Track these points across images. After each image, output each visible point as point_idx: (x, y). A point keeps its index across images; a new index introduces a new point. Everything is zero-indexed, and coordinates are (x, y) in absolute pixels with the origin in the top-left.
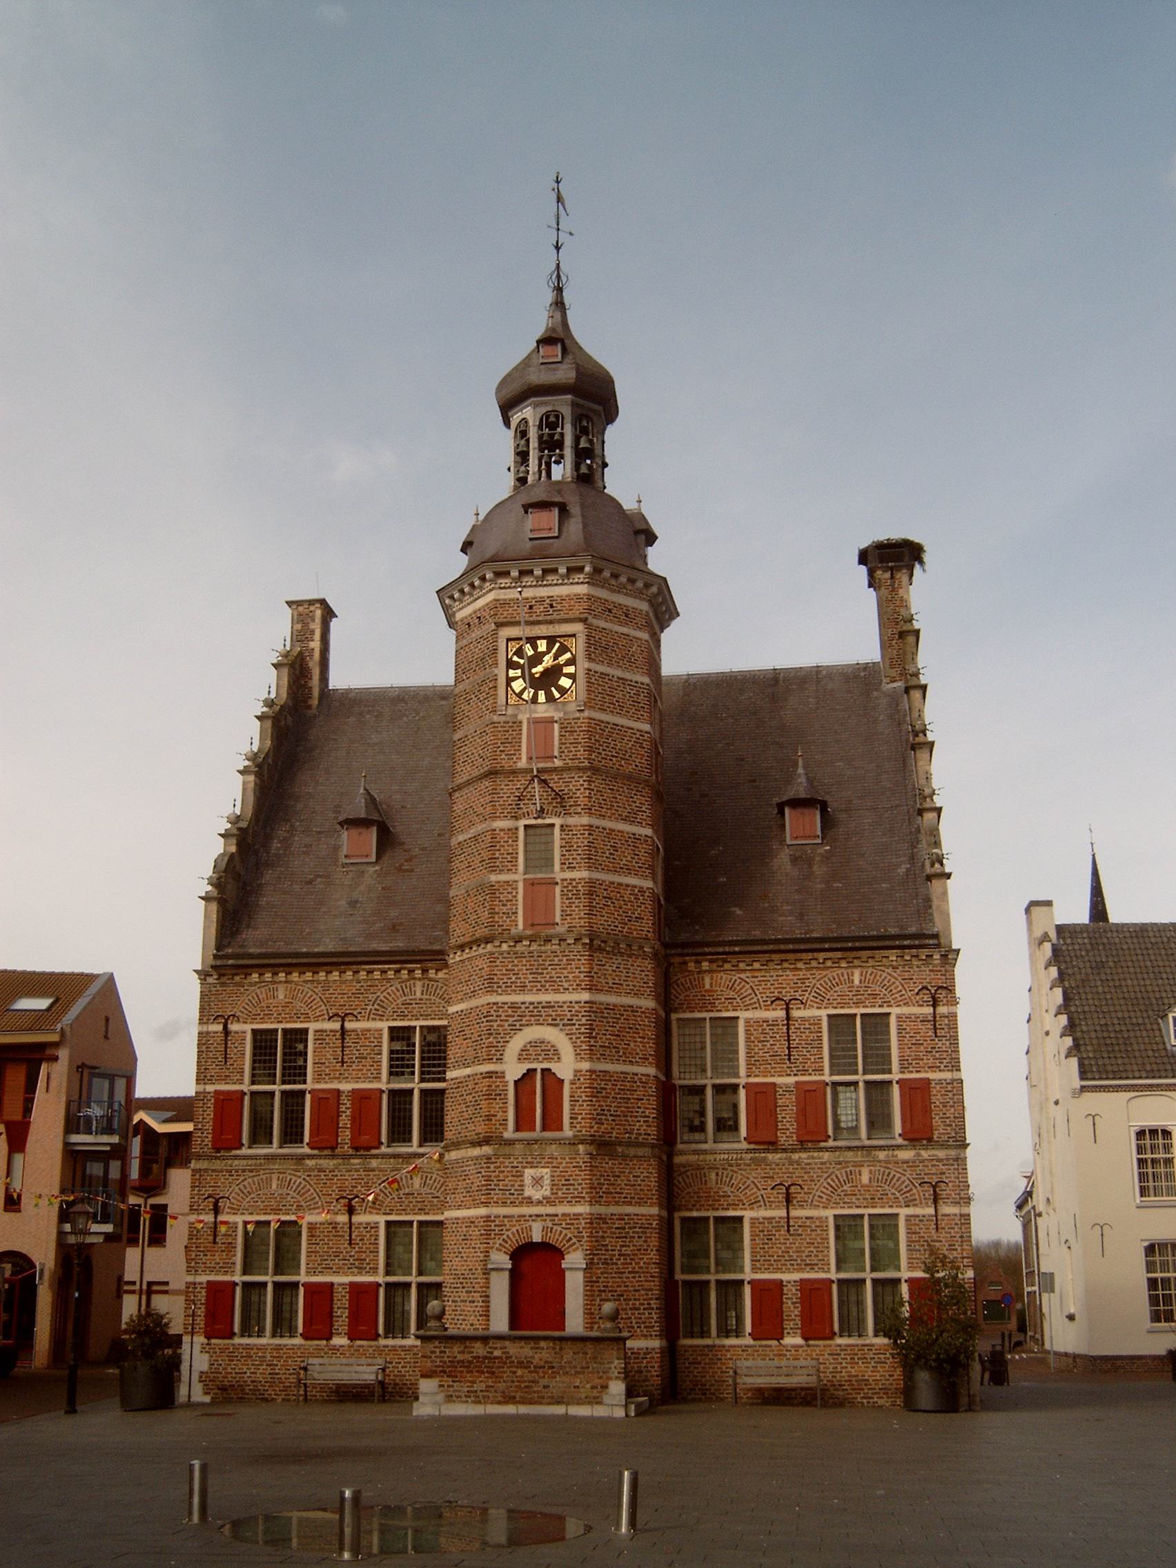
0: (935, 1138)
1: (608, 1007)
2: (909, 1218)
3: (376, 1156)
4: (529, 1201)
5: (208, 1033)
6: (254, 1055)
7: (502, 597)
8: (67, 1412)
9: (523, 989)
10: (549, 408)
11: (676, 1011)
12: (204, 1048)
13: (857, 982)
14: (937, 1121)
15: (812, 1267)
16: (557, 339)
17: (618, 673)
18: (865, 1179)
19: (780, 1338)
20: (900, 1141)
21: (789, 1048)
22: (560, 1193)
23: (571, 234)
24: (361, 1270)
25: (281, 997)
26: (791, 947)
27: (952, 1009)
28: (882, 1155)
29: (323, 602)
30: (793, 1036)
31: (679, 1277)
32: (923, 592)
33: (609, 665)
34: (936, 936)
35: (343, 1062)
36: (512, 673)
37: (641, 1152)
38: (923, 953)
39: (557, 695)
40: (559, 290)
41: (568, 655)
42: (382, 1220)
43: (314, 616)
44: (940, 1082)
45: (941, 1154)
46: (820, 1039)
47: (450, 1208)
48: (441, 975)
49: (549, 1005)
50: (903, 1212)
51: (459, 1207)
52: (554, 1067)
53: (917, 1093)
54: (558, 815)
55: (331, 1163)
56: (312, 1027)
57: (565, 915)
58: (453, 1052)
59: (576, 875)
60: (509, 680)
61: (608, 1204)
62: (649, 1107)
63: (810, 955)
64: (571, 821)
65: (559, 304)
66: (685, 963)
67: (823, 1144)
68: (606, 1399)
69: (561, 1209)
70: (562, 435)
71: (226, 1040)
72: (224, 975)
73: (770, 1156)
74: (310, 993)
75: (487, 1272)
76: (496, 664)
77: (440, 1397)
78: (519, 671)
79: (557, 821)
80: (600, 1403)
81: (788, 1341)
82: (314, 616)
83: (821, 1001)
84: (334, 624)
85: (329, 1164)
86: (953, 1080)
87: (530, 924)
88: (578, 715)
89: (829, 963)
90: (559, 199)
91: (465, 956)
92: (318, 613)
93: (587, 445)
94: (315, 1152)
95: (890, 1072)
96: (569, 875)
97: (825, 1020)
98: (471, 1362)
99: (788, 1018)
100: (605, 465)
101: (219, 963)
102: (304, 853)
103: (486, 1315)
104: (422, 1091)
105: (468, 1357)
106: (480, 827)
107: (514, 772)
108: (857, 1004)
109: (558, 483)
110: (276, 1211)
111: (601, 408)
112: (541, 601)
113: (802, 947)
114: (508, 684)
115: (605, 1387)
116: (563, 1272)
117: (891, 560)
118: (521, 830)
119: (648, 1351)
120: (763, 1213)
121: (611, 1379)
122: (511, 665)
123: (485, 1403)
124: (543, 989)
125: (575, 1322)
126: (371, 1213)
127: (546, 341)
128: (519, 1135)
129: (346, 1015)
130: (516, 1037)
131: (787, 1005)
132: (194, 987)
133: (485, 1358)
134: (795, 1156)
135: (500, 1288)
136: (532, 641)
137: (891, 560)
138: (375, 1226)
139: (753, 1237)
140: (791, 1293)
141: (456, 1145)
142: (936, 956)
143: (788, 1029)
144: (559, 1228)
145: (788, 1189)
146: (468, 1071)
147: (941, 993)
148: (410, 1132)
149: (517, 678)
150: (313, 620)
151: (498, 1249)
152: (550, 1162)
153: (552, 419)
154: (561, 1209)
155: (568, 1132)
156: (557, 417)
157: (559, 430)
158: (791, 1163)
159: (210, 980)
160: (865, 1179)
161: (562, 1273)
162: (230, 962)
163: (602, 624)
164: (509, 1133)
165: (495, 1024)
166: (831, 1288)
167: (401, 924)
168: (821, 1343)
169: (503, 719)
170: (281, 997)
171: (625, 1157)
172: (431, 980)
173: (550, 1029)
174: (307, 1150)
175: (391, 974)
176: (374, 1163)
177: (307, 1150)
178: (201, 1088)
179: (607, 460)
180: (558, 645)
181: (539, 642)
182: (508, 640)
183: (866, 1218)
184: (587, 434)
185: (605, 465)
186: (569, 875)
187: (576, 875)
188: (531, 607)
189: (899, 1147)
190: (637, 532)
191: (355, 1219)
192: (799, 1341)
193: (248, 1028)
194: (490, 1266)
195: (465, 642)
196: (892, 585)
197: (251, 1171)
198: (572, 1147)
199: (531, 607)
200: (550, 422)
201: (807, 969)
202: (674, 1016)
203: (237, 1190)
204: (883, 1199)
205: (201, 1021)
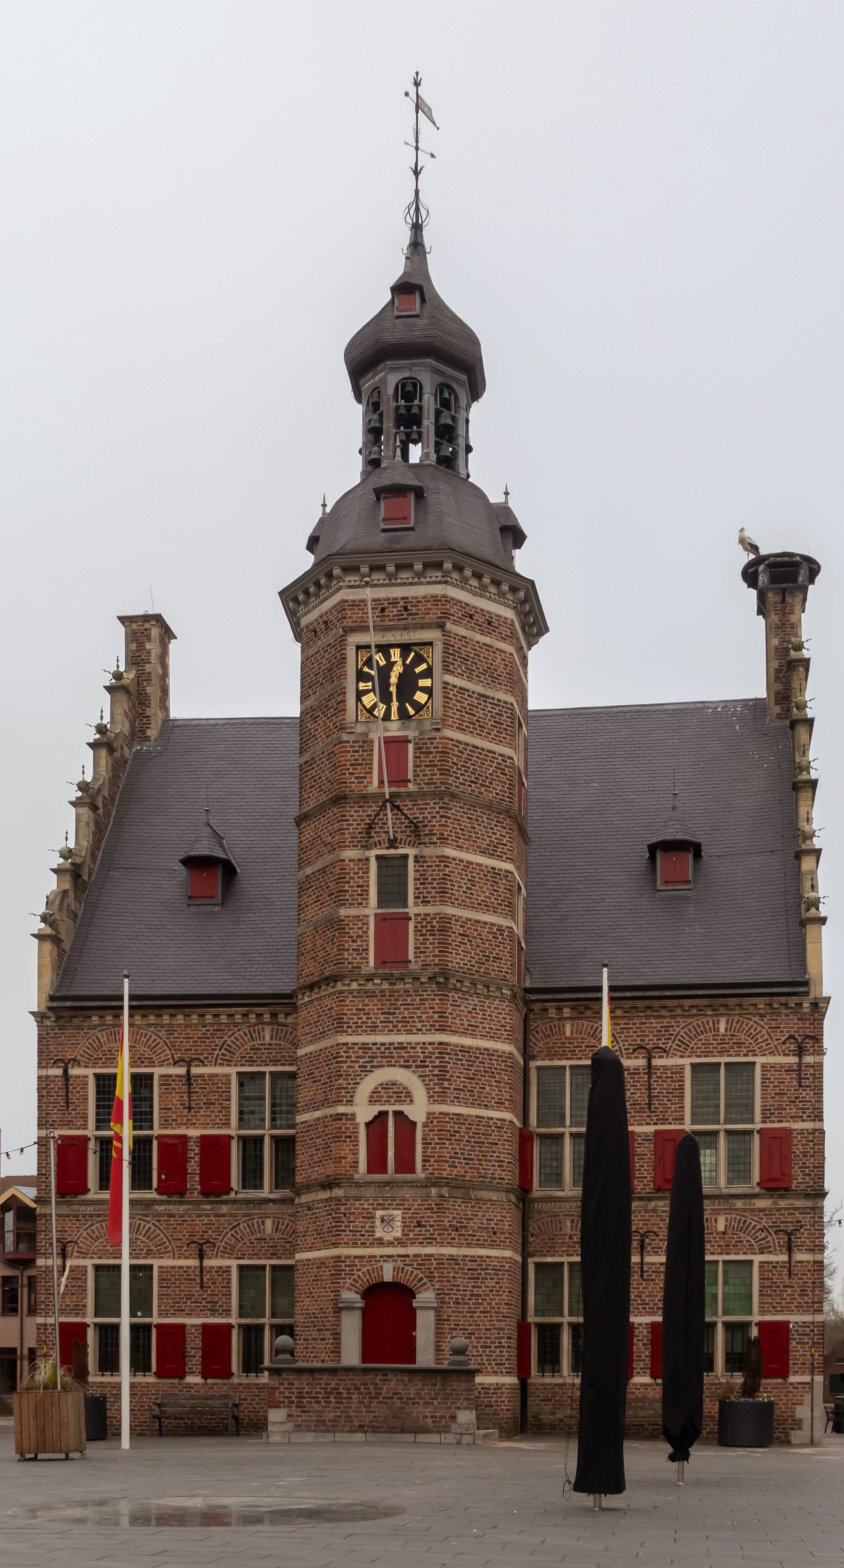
0: (794, 1187)
2: (762, 1264)
4: (380, 1242)
5: (48, 1077)
6: (98, 1100)
7: (351, 597)
9: (374, 1029)
10: (407, 374)
11: (533, 1058)
12: (44, 1093)
13: (722, 1030)
14: (796, 1170)
16: (412, 288)
17: (480, 689)
20: (757, 1190)
21: (649, 1097)
22: (411, 1234)
23: (433, 156)
24: (213, 1312)
27: (817, 1059)
28: (739, 1204)
29: (158, 619)
30: (655, 1085)
31: (532, 1318)
32: (818, 619)
33: (470, 679)
35: (190, 1108)
36: (362, 686)
37: (494, 1196)
38: (793, 1001)
39: (412, 711)
40: (417, 228)
41: (424, 666)
42: (234, 1264)
43: (147, 636)
45: (798, 1204)
46: (681, 1087)
47: (302, 1250)
48: (290, 1020)
49: (401, 1047)
50: (757, 1259)
51: (310, 1249)
53: (777, 1145)
54: (412, 844)
55: (182, 1208)
56: (157, 1071)
58: (304, 1095)
59: (430, 909)
60: (360, 694)
61: (460, 1246)
62: (506, 1151)
63: (675, 1002)
65: (417, 247)
66: (545, 1010)
69: (412, 1250)
71: (67, 1085)
72: (62, 1017)
74: (154, 1037)
75: (338, 1310)
76: (344, 675)
77: (289, 1426)
78: (370, 684)
79: (411, 852)
81: (191, 1379)
82: (147, 636)
83: (684, 1049)
84: (173, 645)
86: (815, 1130)
87: (381, 962)
89: (694, 1011)
90: (419, 106)
91: (314, 996)
92: (155, 632)
93: (449, 422)
94: (164, 1197)
95: (752, 1121)
96: (423, 910)
100: (469, 449)
101: (55, 1004)
103: (337, 1351)
104: (272, 1137)
106: (327, 859)
107: (365, 798)
108: (721, 1053)
109: (415, 466)
111: (464, 377)
112: (394, 602)
113: (668, 993)
114: (359, 699)
115: (453, 1418)
116: (413, 1311)
118: (373, 865)
119: (498, 1387)
122: (361, 676)
123: (334, 1432)
125: (425, 1357)
126: (223, 1257)
127: (402, 289)
129: (193, 1060)
130: (368, 1078)
131: (649, 1052)
132: (32, 1029)
134: (652, 1205)
135: (351, 1330)
136: (384, 649)
138: (228, 1270)
141: (308, 1187)
143: (649, 1078)
144: (410, 1268)
146: (318, 1114)
147: (809, 1042)
148: (261, 1178)
149: (366, 692)
150: (149, 639)
151: (348, 1289)
153: (409, 388)
154: (412, 1250)
156: (414, 385)
157: (416, 402)
159: (48, 1023)
161: (412, 1314)
162: (68, 1004)
163: (462, 631)
165: (345, 1065)
169: (352, 738)
171: (478, 1200)
173: (402, 1071)
175: (238, 1018)
176: (225, 1209)
178: (43, 1133)
179: (472, 443)
180: (413, 654)
181: (392, 651)
182: (359, 648)
183: (721, 1264)
184: (449, 408)
185: (469, 449)
186: (423, 910)
187: (430, 909)
188: (383, 610)
190: (504, 530)
191: (207, 1263)
193: (90, 1072)
194: (341, 1305)
195: (311, 652)
197: (99, 1216)
198: (425, 1190)
199: (383, 610)
200: (409, 391)
201: (672, 1017)
202: (533, 1064)
203: (85, 1234)
204: (737, 1247)
205: (40, 1066)
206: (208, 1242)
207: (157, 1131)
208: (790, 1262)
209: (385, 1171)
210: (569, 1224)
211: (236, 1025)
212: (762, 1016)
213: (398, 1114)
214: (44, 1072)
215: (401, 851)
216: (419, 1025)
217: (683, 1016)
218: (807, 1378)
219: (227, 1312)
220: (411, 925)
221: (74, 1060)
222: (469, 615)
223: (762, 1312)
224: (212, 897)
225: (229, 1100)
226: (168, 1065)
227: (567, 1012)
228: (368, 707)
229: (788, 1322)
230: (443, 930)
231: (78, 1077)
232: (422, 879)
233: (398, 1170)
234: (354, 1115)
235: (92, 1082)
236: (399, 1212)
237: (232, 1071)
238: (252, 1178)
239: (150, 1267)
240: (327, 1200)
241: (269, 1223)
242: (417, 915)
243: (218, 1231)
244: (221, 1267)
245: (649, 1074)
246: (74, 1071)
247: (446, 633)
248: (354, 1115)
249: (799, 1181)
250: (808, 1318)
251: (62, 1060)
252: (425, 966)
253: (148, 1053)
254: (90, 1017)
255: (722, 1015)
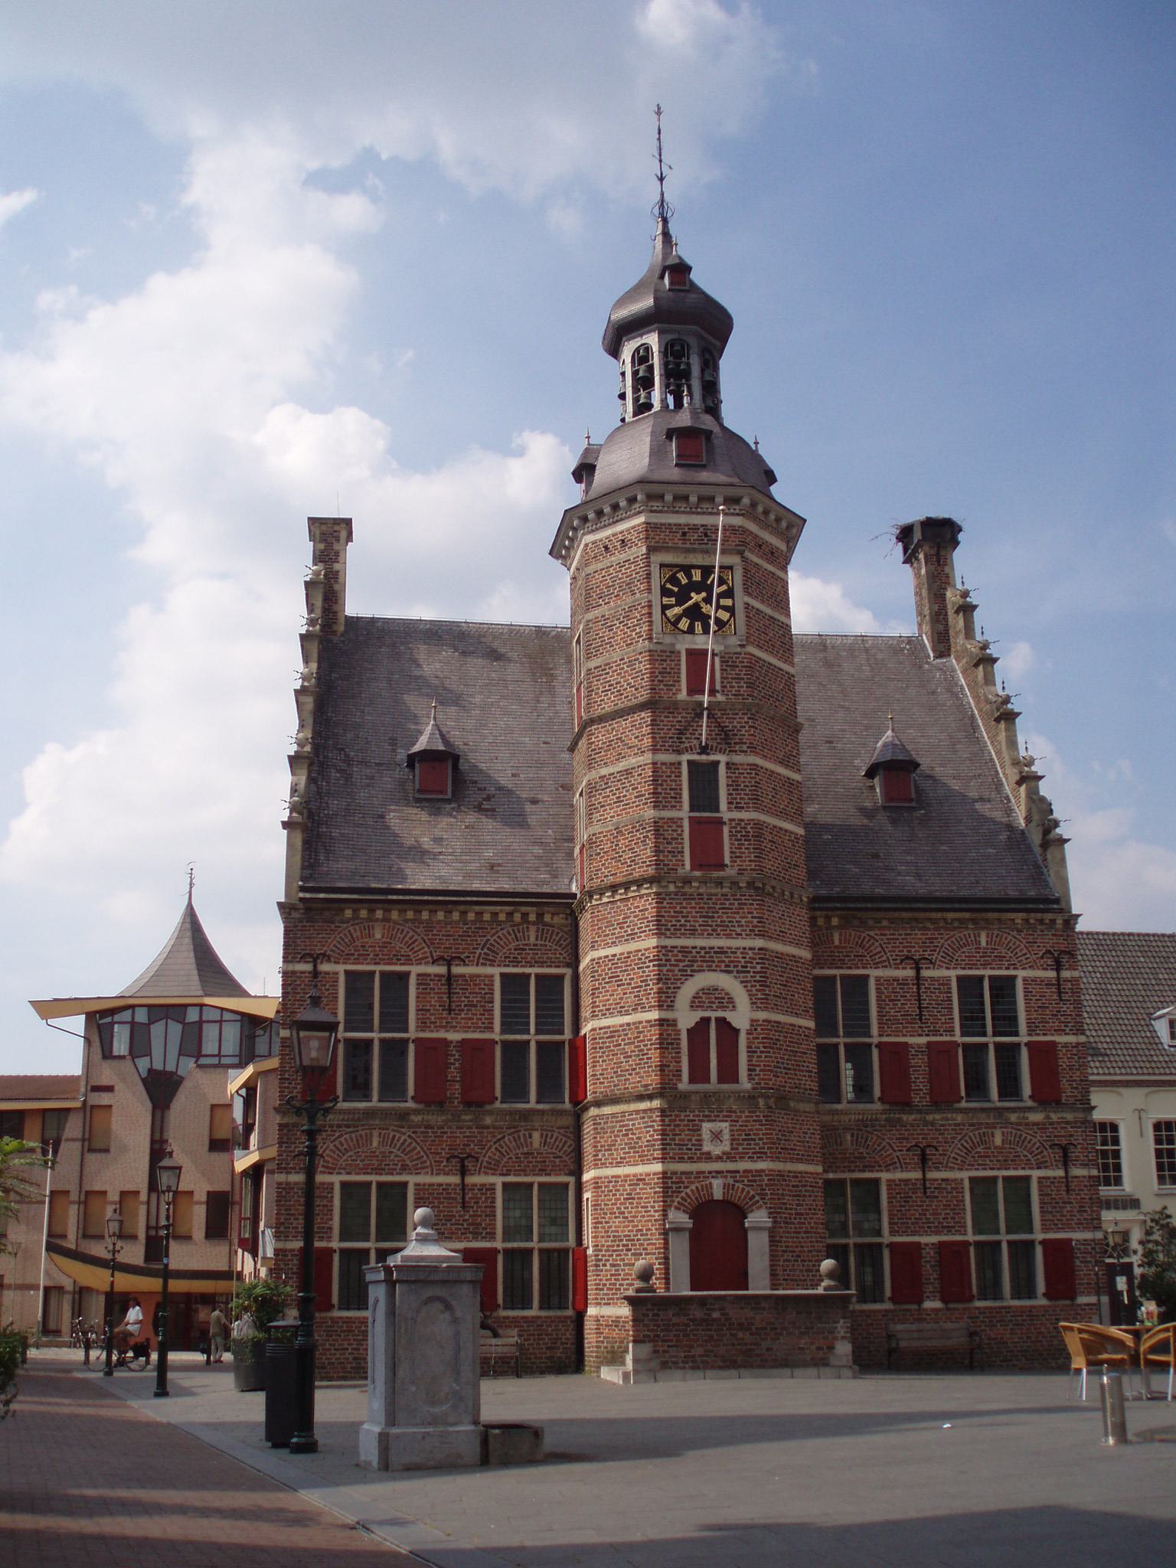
1: (780, 956)
3: (490, 1113)
4: (708, 1157)
5: (294, 972)
8: (157, 1395)
9: (693, 932)
10: (675, 336)
13: (983, 944)
15: (949, 1229)
18: (998, 1141)
19: (920, 1302)
20: (1030, 1103)
21: (920, 1008)
24: (476, 1236)
25: (378, 936)
26: (921, 905)
28: (1013, 1117)
32: (967, 566)
34: (1057, 901)
40: (665, 221)
42: (498, 1181)
44: (1065, 1045)
45: (1069, 1117)
46: (949, 999)
49: (721, 951)
50: (1036, 1174)
52: (729, 1016)
55: (441, 1119)
57: (734, 857)
59: (744, 815)
63: (939, 915)
64: (738, 759)
67: (957, 1105)
68: (833, 1361)
69: (742, 1166)
70: (688, 365)
73: (905, 1117)
79: (722, 759)
80: (827, 1365)
81: (928, 1304)
82: (330, 536)
85: (435, 1119)
88: (739, 650)
97: (954, 980)
98: (687, 1325)
99: (918, 977)
102: (368, 785)
105: (684, 1319)
108: (985, 966)
110: (378, 1171)
112: (695, 528)
114: (663, 613)
115: (831, 1348)
116: (745, 1231)
117: (931, 541)
120: (899, 1175)
121: (836, 1339)
124: (714, 933)
126: (486, 1173)
128: (541, 1106)
131: (917, 963)
133: (704, 1320)
134: (930, 1117)
137: (931, 541)
138: (492, 1188)
139: (890, 1197)
140: (929, 1255)
142: (1059, 921)
143: (918, 989)
145: (462, 1160)
146: (627, 1019)
152: (729, 1115)
154: (742, 1166)
155: (745, 1084)
156: (683, 347)
158: (926, 1123)
160: (998, 1141)
162: (322, 896)
164: (684, 1085)
166: (968, 1252)
167: (499, 865)
168: (960, 1306)
170: (378, 936)
172: (546, 924)
173: (723, 976)
174: (411, 1104)
176: (488, 1120)
177: (411, 1104)
187: (744, 815)
188: (684, 534)
189: (1030, 1109)
191: (471, 1180)
192: (937, 1304)
193: (341, 968)
196: (938, 561)
197: (348, 1126)
199: (684, 534)
201: (935, 929)
203: (331, 1146)
204: (1016, 1163)
206: (470, 1156)
207: (412, 1033)
208: (1066, 1177)
209: (707, 1080)
210: (849, 1137)
211: (500, 923)
212: (1019, 931)
213: (722, 1022)
214: (291, 967)
215: (712, 758)
216: (738, 930)
217: (946, 929)
218: (1093, 1299)
219: (492, 1236)
220: (726, 830)
221: (324, 955)
222: (760, 545)
223: (1045, 1229)
224: (441, 792)
225: (492, 1002)
226: (427, 963)
227: (835, 921)
228: (356, 604)
229: (1070, 1240)
230: (758, 836)
231: (327, 973)
232: (734, 785)
233: (720, 1080)
234: (675, 1020)
235: (342, 978)
236: (727, 1124)
237: (496, 971)
238: (515, 1088)
239: (876, 1182)
240: (645, 1111)
241: (536, 1135)
242: (731, 820)
243: (480, 1144)
244: (484, 1185)
245: (918, 985)
246: (325, 967)
247: (745, 560)
248: (675, 1020)
249: (1067, 1093)
250: (1088, 1235)
251: (311, 955)
252: (741, 872)
253: (405, 950)
254: (343, 910)
255: (983, 928)
